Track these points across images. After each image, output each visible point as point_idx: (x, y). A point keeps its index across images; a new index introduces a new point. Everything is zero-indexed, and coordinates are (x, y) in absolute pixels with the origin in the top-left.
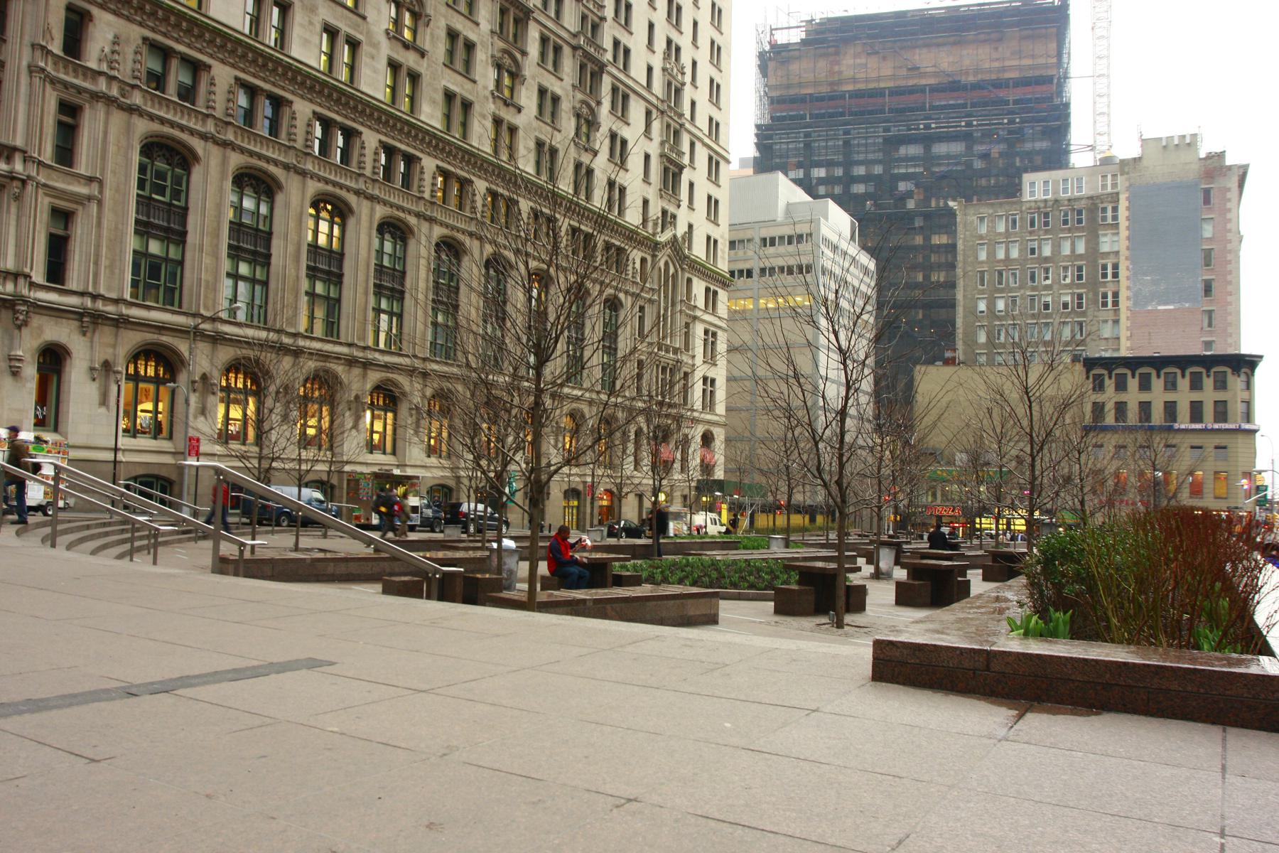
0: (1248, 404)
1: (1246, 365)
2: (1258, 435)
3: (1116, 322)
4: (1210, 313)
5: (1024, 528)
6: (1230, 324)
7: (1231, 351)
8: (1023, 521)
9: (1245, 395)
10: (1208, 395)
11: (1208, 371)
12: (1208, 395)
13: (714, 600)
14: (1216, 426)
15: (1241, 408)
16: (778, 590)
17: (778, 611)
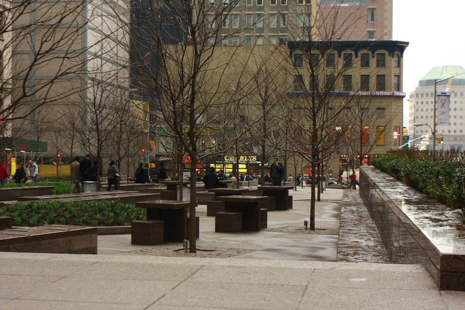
0: (399, 77)
1: (398, 48)
2: (404, 99)
3: (309, 15)
4: (373, 10)
5: (231, 170)
6: (386, 19)
7: (386, 39)
8: (244, 166)
9: (396, 71)
10: (373, 70)
11: (373, 53)
12: (373, 70)
13: (93, 235)
14: (378, 93)
15: (394, 80)
16: (134, 225)
17: (135, 242)
